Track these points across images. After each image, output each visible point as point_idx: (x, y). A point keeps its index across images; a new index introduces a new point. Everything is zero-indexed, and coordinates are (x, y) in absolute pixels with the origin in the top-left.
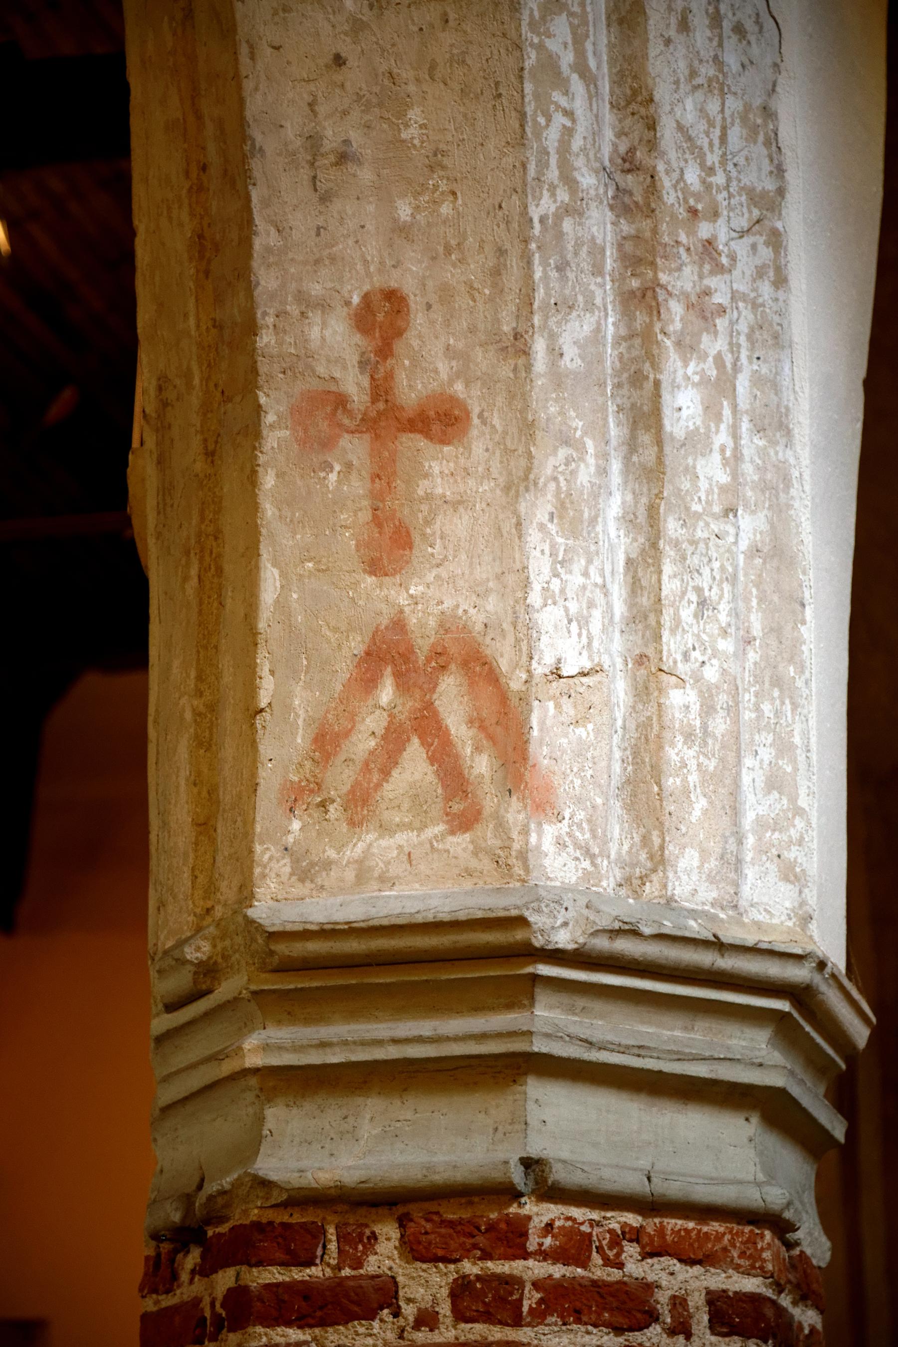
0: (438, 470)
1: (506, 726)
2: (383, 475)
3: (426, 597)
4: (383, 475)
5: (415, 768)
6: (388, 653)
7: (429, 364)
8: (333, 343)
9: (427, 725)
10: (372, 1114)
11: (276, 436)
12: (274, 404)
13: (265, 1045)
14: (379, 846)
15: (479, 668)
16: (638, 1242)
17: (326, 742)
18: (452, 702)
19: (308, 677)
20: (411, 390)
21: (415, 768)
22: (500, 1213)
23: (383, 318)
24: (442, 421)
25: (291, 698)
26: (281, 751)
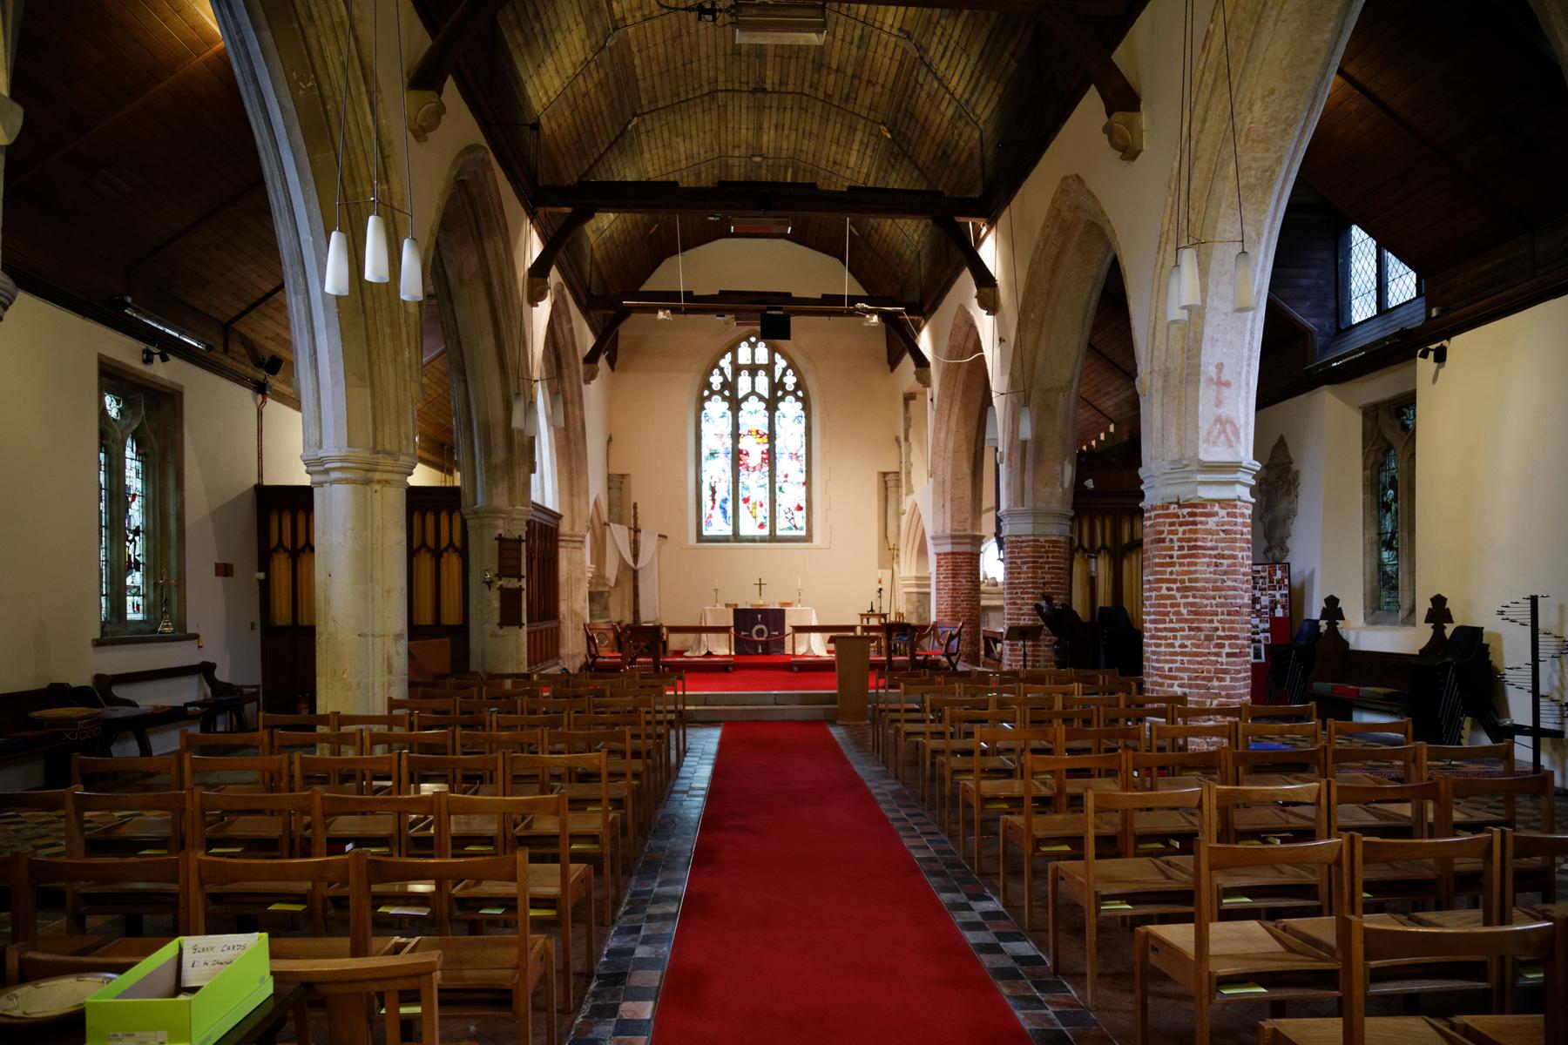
0: (1226, 392)
1: (1236, 432)
2: (1218, 392)
3: (1225, 411)
4: (1218, 392)
5: (1223, 438)
6: (1218, 420)
7: (1227, 375)
8: (1212, 371)
9: (1224, 431)
10: (1214, 488)
11: (1202, 384)
12: (1202, 379)
13: (1200, 477)
14: (1218, 450)
15: (1232, 424)
16: (586, 667)
17: (1209, 433)
18: (1228, 428)
19: (862, 52)
20: (1223, 379)
21: (1223, 438)
22: (136, 532)
23: (1220, 367)
24: (1228, 384)
25: (1204, 426)
26: (1202, 433)
